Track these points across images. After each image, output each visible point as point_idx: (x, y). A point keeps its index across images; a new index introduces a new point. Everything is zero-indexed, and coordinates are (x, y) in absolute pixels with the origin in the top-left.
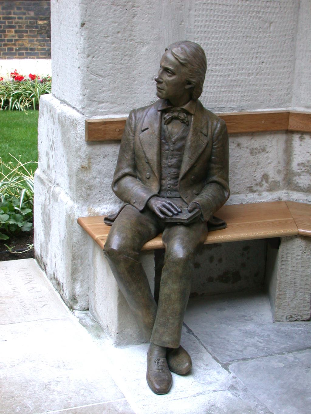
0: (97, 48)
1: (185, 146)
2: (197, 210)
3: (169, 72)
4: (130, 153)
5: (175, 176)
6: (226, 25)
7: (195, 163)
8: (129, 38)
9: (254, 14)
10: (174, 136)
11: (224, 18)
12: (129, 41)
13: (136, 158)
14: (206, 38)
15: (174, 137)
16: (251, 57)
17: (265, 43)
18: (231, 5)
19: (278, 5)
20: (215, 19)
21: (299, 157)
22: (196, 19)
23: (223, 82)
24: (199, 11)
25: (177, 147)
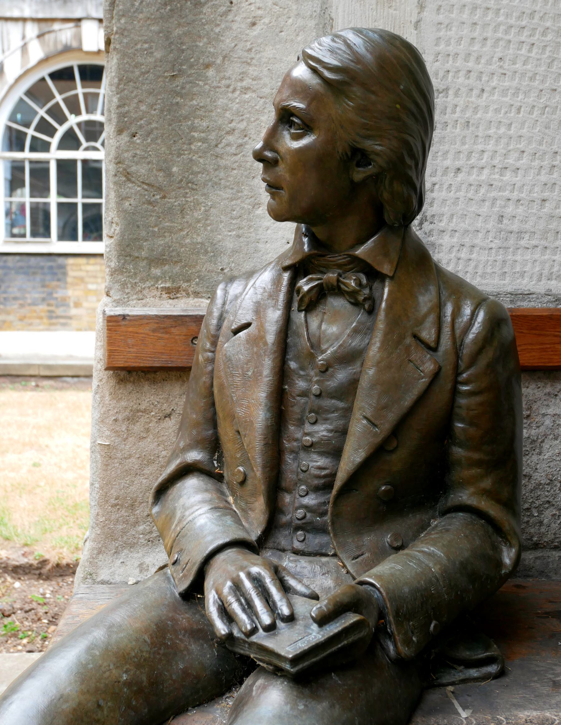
0: (143, 108)
1: (358, 381)
2: (352, 618)
5: (322, 481)
7: (386, 441)
8: (239, 84)
10: (324, 347)
11: (526, 33)
12: (238, 92)
14: (471, 90)
15: (325, 351)
20: (500, 35)
23: (524, 221)
24: (451, 11)
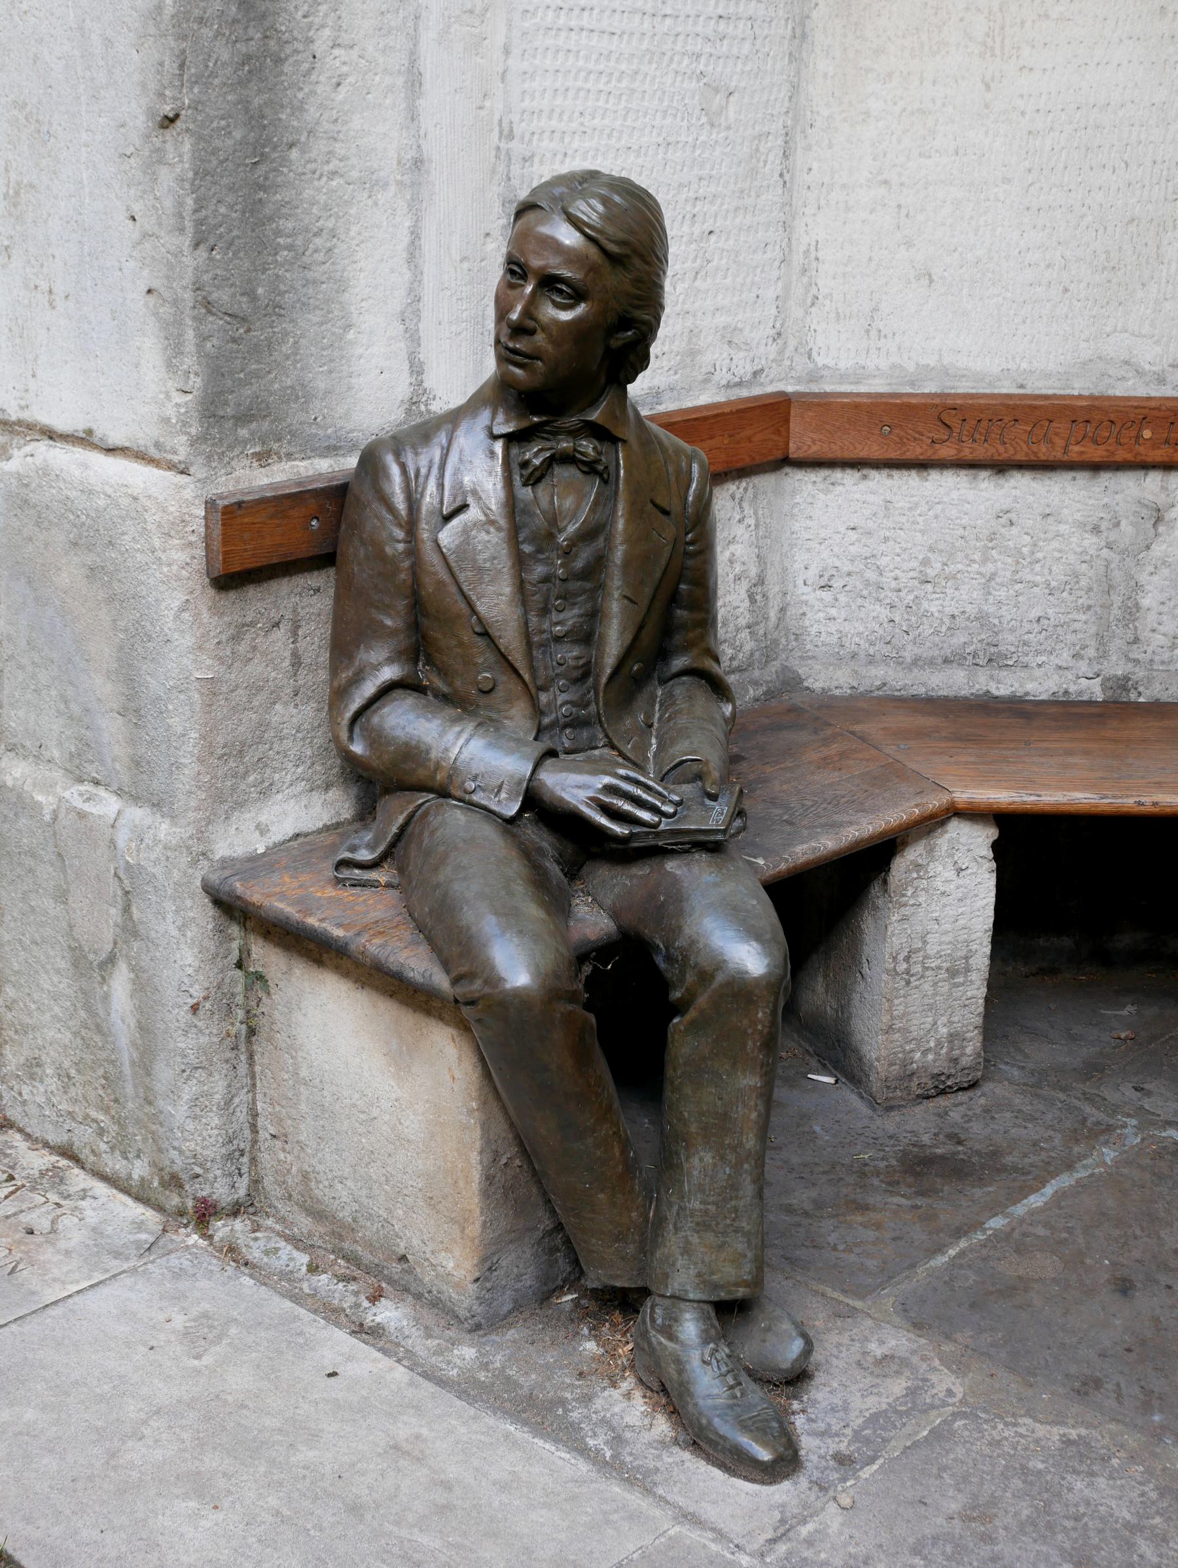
3: (561, 291)
4: (400, 608)
6: (609, 106)
8: (326, 168)
9: (686, 61)
11: (604, 79)
12: (324, 179)
13: (425, 622)
15: (565, 529)
16: (680, 217)
17: (717, 166)
18: (623, 33)
19: (749, 32)
21: (823, 547)
22: (526, 86)
25: (579, 564)
